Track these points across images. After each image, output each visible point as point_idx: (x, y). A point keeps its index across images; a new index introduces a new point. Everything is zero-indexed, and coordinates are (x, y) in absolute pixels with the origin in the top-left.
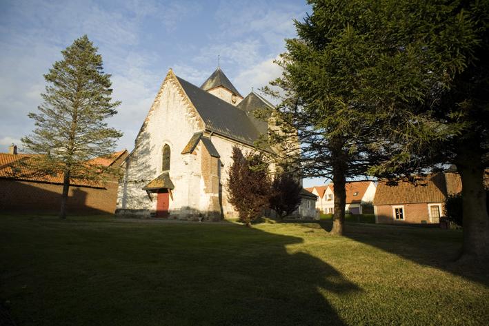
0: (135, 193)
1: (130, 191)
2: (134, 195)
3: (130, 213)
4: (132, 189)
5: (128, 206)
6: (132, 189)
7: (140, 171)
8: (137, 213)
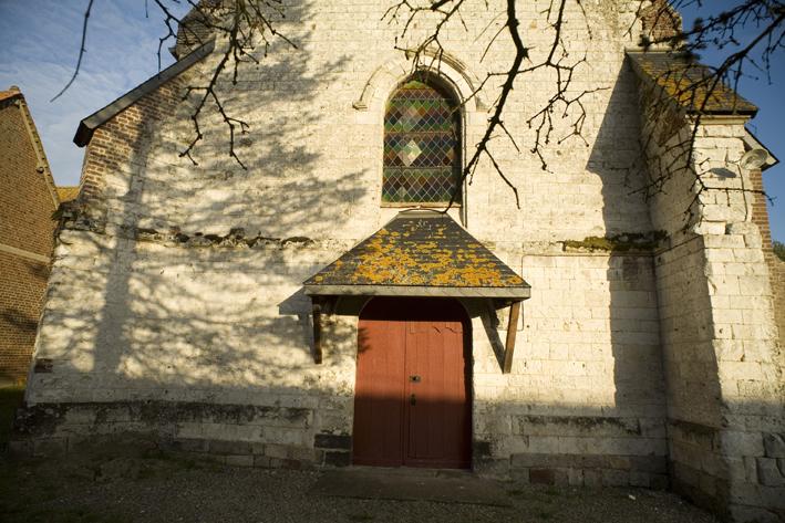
0: (183, 292)
1: (154, 282)
2: (173, 304)
3: (139, 426)
4: (169, 272)
5: (132, 367)
6: (169, 272)
7: (225, 175)
8: (189, 431)
